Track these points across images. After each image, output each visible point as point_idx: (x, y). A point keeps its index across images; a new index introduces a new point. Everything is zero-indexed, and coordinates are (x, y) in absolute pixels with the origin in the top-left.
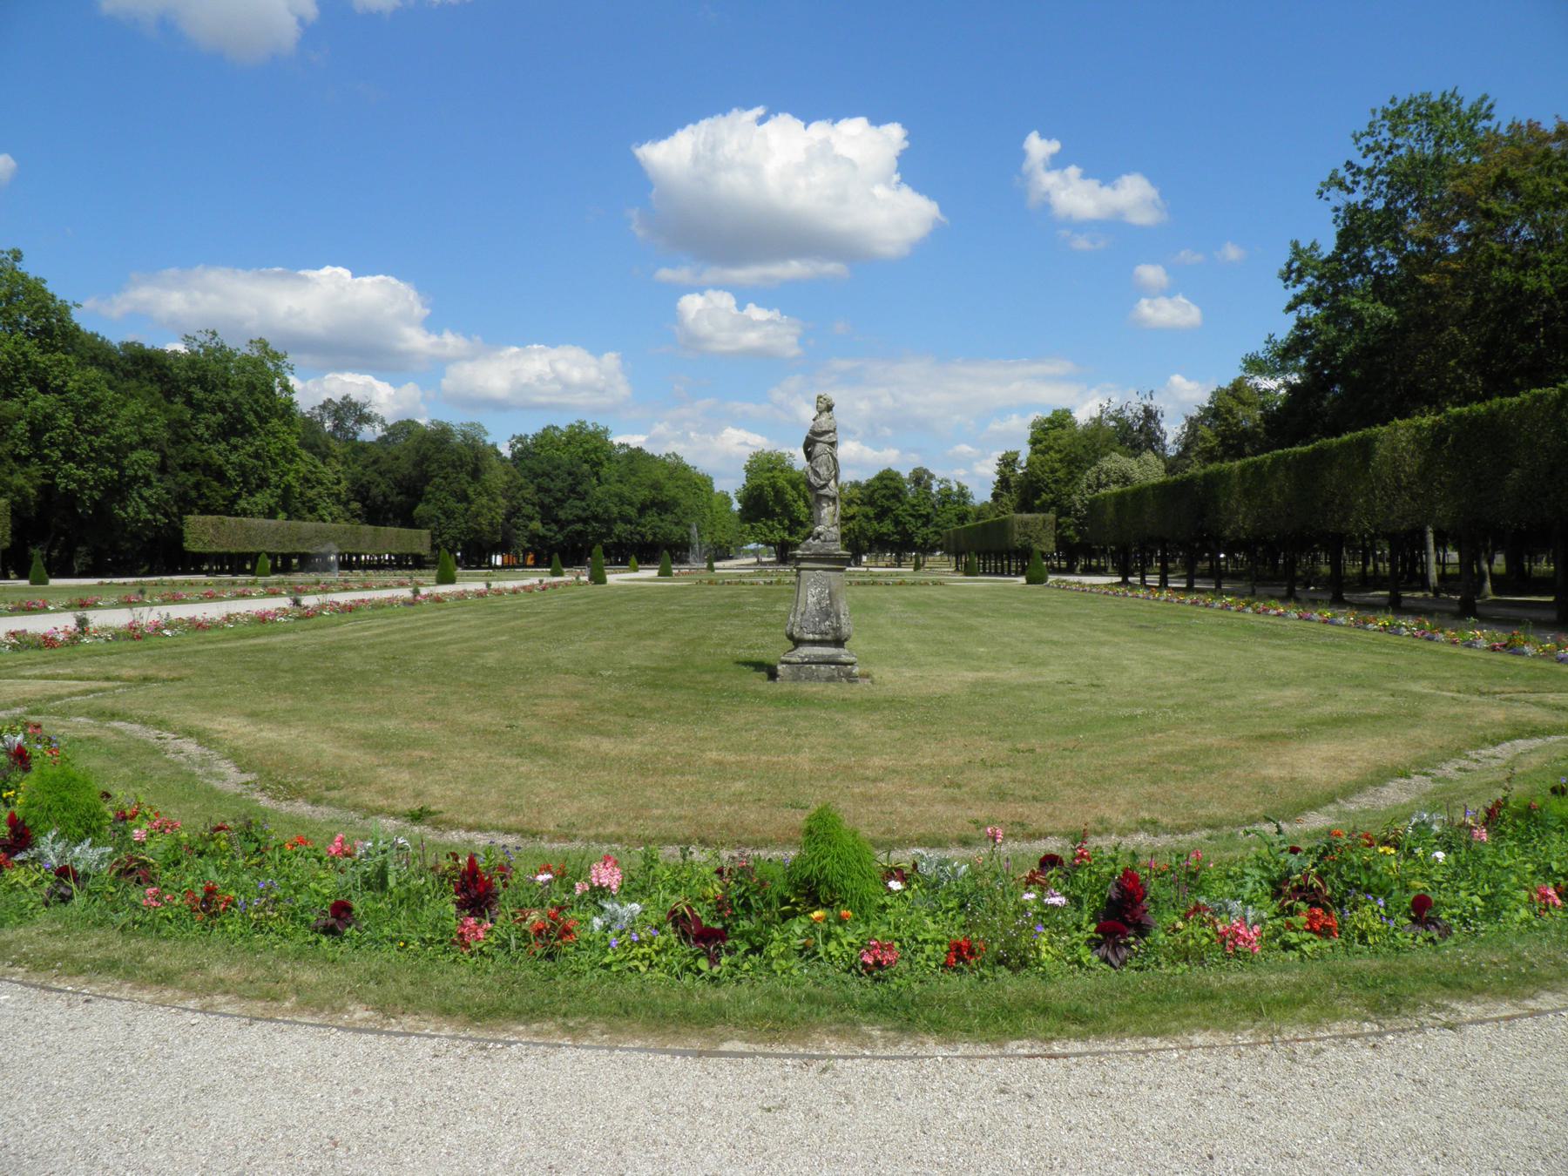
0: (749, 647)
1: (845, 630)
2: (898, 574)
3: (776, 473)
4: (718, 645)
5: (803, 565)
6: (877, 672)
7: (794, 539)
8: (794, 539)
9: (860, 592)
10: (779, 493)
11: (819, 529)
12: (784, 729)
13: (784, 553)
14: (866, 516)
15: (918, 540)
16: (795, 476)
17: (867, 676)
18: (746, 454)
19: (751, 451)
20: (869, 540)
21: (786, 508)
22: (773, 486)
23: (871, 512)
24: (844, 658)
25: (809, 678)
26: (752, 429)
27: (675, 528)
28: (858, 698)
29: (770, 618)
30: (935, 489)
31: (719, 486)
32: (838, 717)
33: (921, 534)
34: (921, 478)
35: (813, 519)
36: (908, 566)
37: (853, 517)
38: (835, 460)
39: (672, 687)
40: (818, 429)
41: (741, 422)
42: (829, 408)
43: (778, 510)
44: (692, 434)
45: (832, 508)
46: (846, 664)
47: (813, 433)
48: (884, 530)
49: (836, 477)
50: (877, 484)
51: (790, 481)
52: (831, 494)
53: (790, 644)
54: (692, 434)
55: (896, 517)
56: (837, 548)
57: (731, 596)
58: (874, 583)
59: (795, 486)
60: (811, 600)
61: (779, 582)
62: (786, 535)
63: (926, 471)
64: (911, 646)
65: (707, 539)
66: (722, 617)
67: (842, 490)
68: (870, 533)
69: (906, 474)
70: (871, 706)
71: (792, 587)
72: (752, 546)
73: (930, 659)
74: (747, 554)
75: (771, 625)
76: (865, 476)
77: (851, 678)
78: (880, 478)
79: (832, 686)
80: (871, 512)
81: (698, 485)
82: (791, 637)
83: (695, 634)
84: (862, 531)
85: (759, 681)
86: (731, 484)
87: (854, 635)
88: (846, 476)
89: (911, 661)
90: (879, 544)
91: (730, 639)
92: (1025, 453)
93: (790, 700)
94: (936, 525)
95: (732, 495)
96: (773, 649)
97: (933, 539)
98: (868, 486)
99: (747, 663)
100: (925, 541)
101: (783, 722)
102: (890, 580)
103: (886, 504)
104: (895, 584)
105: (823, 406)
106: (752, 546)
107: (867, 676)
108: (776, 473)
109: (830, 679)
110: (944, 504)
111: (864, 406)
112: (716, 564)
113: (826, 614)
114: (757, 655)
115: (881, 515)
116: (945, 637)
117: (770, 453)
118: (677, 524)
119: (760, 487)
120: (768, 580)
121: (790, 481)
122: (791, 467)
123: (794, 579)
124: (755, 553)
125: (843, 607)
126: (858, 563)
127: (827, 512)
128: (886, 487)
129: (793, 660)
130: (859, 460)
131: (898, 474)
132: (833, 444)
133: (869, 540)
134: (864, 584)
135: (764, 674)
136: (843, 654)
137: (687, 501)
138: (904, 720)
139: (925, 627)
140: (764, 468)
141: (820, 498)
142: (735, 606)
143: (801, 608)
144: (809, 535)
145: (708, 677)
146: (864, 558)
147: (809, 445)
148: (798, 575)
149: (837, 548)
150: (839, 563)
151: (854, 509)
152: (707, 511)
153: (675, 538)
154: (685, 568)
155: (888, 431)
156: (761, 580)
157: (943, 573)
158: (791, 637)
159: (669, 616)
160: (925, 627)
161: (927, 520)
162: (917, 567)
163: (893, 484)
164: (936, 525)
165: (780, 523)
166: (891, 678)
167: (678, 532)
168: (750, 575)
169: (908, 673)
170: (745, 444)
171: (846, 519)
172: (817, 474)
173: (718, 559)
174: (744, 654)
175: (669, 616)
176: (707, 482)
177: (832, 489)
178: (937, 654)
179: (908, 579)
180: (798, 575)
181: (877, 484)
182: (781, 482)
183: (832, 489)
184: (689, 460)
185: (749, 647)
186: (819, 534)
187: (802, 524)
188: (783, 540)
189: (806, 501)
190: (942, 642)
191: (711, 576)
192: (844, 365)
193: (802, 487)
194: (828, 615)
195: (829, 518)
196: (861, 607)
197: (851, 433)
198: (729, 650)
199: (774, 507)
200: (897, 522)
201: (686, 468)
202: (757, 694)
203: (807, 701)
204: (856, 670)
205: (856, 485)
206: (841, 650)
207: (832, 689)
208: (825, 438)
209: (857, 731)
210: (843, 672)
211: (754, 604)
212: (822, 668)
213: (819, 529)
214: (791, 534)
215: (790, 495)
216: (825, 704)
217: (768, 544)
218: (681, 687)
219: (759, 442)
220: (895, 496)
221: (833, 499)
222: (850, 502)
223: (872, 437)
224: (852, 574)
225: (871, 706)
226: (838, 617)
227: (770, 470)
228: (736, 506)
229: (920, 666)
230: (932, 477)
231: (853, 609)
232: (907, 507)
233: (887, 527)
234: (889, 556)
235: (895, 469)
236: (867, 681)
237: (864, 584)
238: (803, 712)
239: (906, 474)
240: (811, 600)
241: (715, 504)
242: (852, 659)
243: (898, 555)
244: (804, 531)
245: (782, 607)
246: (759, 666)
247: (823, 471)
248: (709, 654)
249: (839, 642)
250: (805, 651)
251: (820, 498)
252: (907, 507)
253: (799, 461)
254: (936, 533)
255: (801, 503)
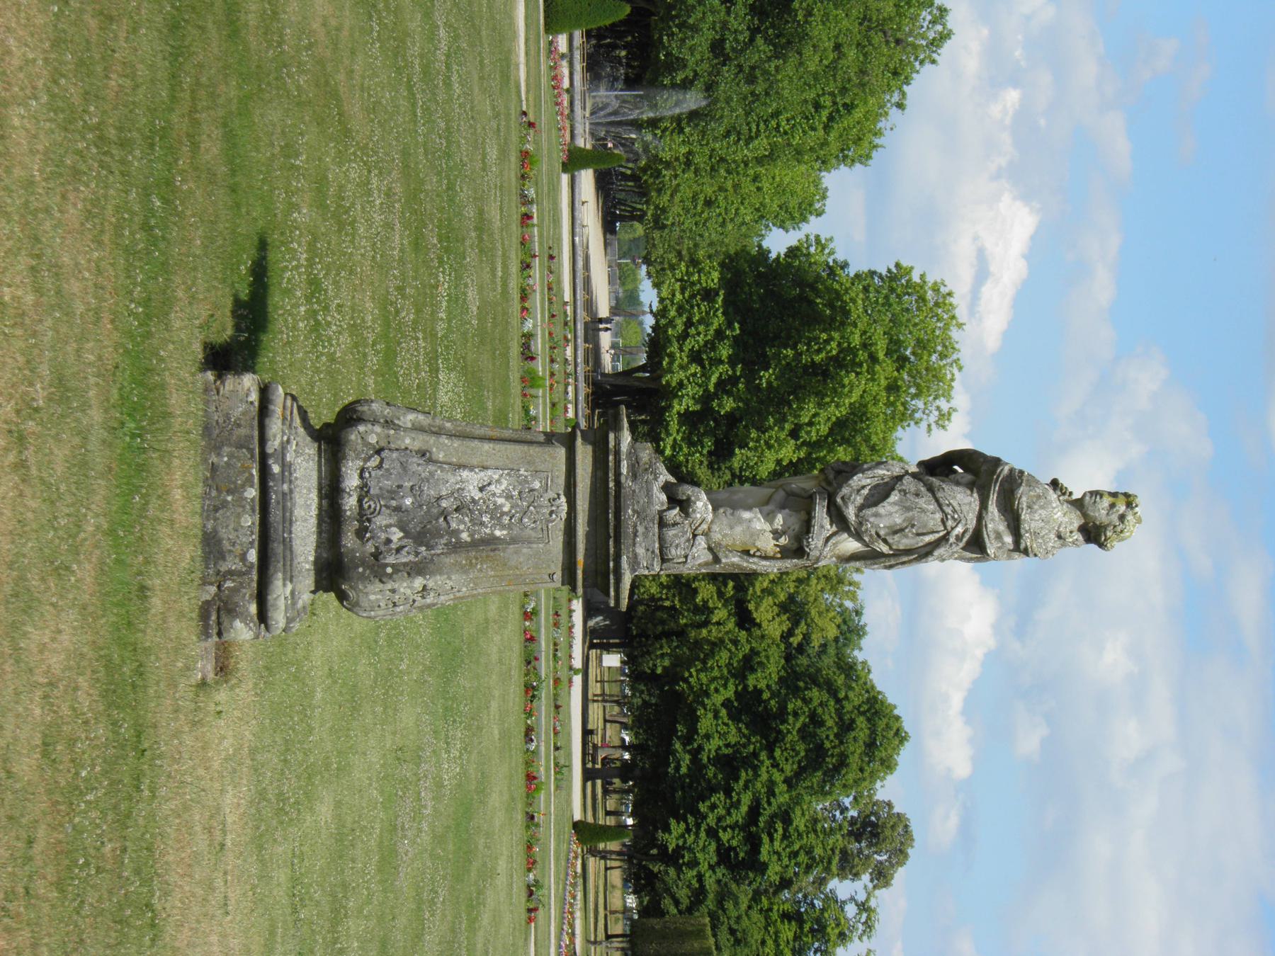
0: (314, 283)
1: (374, 593)
2: (562, 769)
3: (886, 369)
4: (321, 183)
5: (584, 454)
6: (236, 698)
7: (674, 431)
8: (674, 431)
9: (503, 645)
10: (820, 378)
11: (702, 505)
12: (40, 394)
13: (627, 398)
14: (749, 664)
15: (674, 835)
16: (878, 427)
17: (223, 669)
18: (949, 269)
19: (958, 282)
20: (673, 675)
21: (774, 403)
22: (844, 361)
23: (765, 678)
24: (280, 591)
25: (217, 483)
26: (1026, 299)
27: (701, 42)
28: (150, 638)
29: (413, 350)
30: (842, 888)
31: (841, 183)
32: (85, 572)
33: (696, 844)
34: (877, 839)
35: (734, 486)
36: (591, 802)
37: (745, 620)
38: (925, 553)
39: (174, 27)
40: (1024, 496)
41: (1052, 258)
42: (1093, 533)
43: (766, 377)
44: (1012, 96)
45: (768, 544)
46: (262, 598)
47: (1014, 480)
48: (706, 723)
49: (870, 557)
50: (856, 698)
51: (859, 415)
52: (815, 543)
53: (324, 415)
54: (1012, 96)
55: (751, 762)
56: (639, 562)
57: (482, 225)
58: (530, 691)
59: (845, 429)
60: (471, 481)
61: (529, 380)
62: (685, 403)
63: (900, 855)
64: (325, 811)
65: (670, 147)
66: (413, 196)
67: (836, 582)
68: (696, 677)
69: (890, 790)
70: (123, 679)
71: (515, 419)
72: (649, 295)
73: (281, 876)
74: (620, 276)
75: (390, 357)
76: (880, 658)
77: (215, 615)
78: (875, 709)
79: (190, 553)
80: (765, 678)
81: (844, 121)
82: (349, 416)
83: (355, 109)
84: (703, 652)
85: (202, 313)
86: (850, 222)
87: (359, 624)
88: (879, 596)
89: (275, 811)
90: (659, 709)
91: (343, 223)
92: (852, 271)
93: (139, 409)
94: (723, 896)
95: (813, 226)
96: (307, 362)
97: (681, 884)
98: (849, 669)
99: (260, 273)
100: (672, 858)
101: (63, 389)
102: (542, 744)
103: (791, 728)
104: (530, 759)
105: (1101, 512)
106: (649, 295)
107: (223, 669)
108: (886, 369)
109: (212, 546)
110: (794, 917)
111: (1111, 659)
112: (587, 179)
113: (426, 531)
114: (289, 310)
115: (748, 709)
116: (354, 926)
117: (948, 348)
118: (717, 47)
119: (839, 316)
120: (539, 345)
121: (859, 415)
122: (903, 416)
123: (544, 425)
124: (626, 304)
125: (449, 584)
126: (597, 641)
127: (754, 532)
128: (846, 727)
129: (275, 426)
130: (934, 635)
131: (888, 765)
132: (976, 545)
133: (673, 675)
134: (530, 660)
135: (225, 331)
136: (294, 588)
137: (790, 82)
138: (75, 790)
139: (388, 859)
140: (902, 328)
141: (802, 506)
142: (450, 238)
143: (443, 449)
144: (682, 475)
145: (211, 149)
146: (613, 660)
147: (969, 468)
148: (550, 438)
149: (639, 562)
150: (593, 568)
151: (771, 622)
152: (761, 145)
153: (672, 44)
154: (572, 74)
155: (1029, 741)
156: (536, 323)
157: (566, 916)
158: (349, 416)
159: (415, 23)
160: (388, 859)
161: (742, 862)
162: (586, 833)
163: (855, 750)
164: (723, 896)
165: (724, 386)
166: (218, 745)
167: (693, 50)
168: (552, 289)
169: (233, 802)
170: (982, 274)
171: (737, 586)
172: (880, 494)
173: (603, 183)
174: (290, 272)
175: (415, 23)
176: (855, 146)
177: (831, 546)
178: (297, 900)
179: (546, 802)
180: (550, 438)
181: (856, 698)
182: (856, 387)
183: (831, 546)
184: (926, 84)
185: (314, 283)
186: (685, 506)
187: (721, 453)
188: (672, 393)
189: (795, 468)
190: (337, 914)
191: (549, 149)
192: (1247, 595)
193: (843, 454)
194: (421, 536)
195: (737, 535)
196: (452, 655)
197: (1019, 618)
198: (304, 215)
199: (780, 365)
200: (731, 764)
201: (899, 74)
202: (156, 308)
203: (135, 475)
204: (242, 631)
205: (851, 630)
206: (308, 581)
207: (177, 552)
208: (995, 521)
209: (35, 635)
210: (238, 588)
211: (457, 300)
212: (249, 521)
213: (702, 505)
214: (686, 417)
215: (819, 417)
216: (130, 527)
217: (657, 345)
218: (177, 55)
219: (984, 325)
220: (816, 757)
221: (797, 550)
222: (794, 610)
223: (1020, 683)
224: (559, 618)
225: (123, 679)
226: (416, 569)
227: (894, 347)
228: (777, 242)
229: (259, 843)
230: (882, 876)
231: (445, 618)
232: (783, 797)
233: (717, 732)
234: (619, 739)
235: (904, 756)
236: (205, 668)
237: (530, 660)
238: (99, 459)
239: (890, 790)
240: (471, 481)
241: (787, 173)
242: (279, 617)
243: (625, 771)
244: (697, 461)
245: (448, 390)
246: (253, 314)
247: (889, 513)
248: (289, 151)
249: (333, 574)
250: (304, 465)
251: (802, 506)
252: (783, 797)
253: (917, 443)
254: (699, 895)
255: (789, 452)
